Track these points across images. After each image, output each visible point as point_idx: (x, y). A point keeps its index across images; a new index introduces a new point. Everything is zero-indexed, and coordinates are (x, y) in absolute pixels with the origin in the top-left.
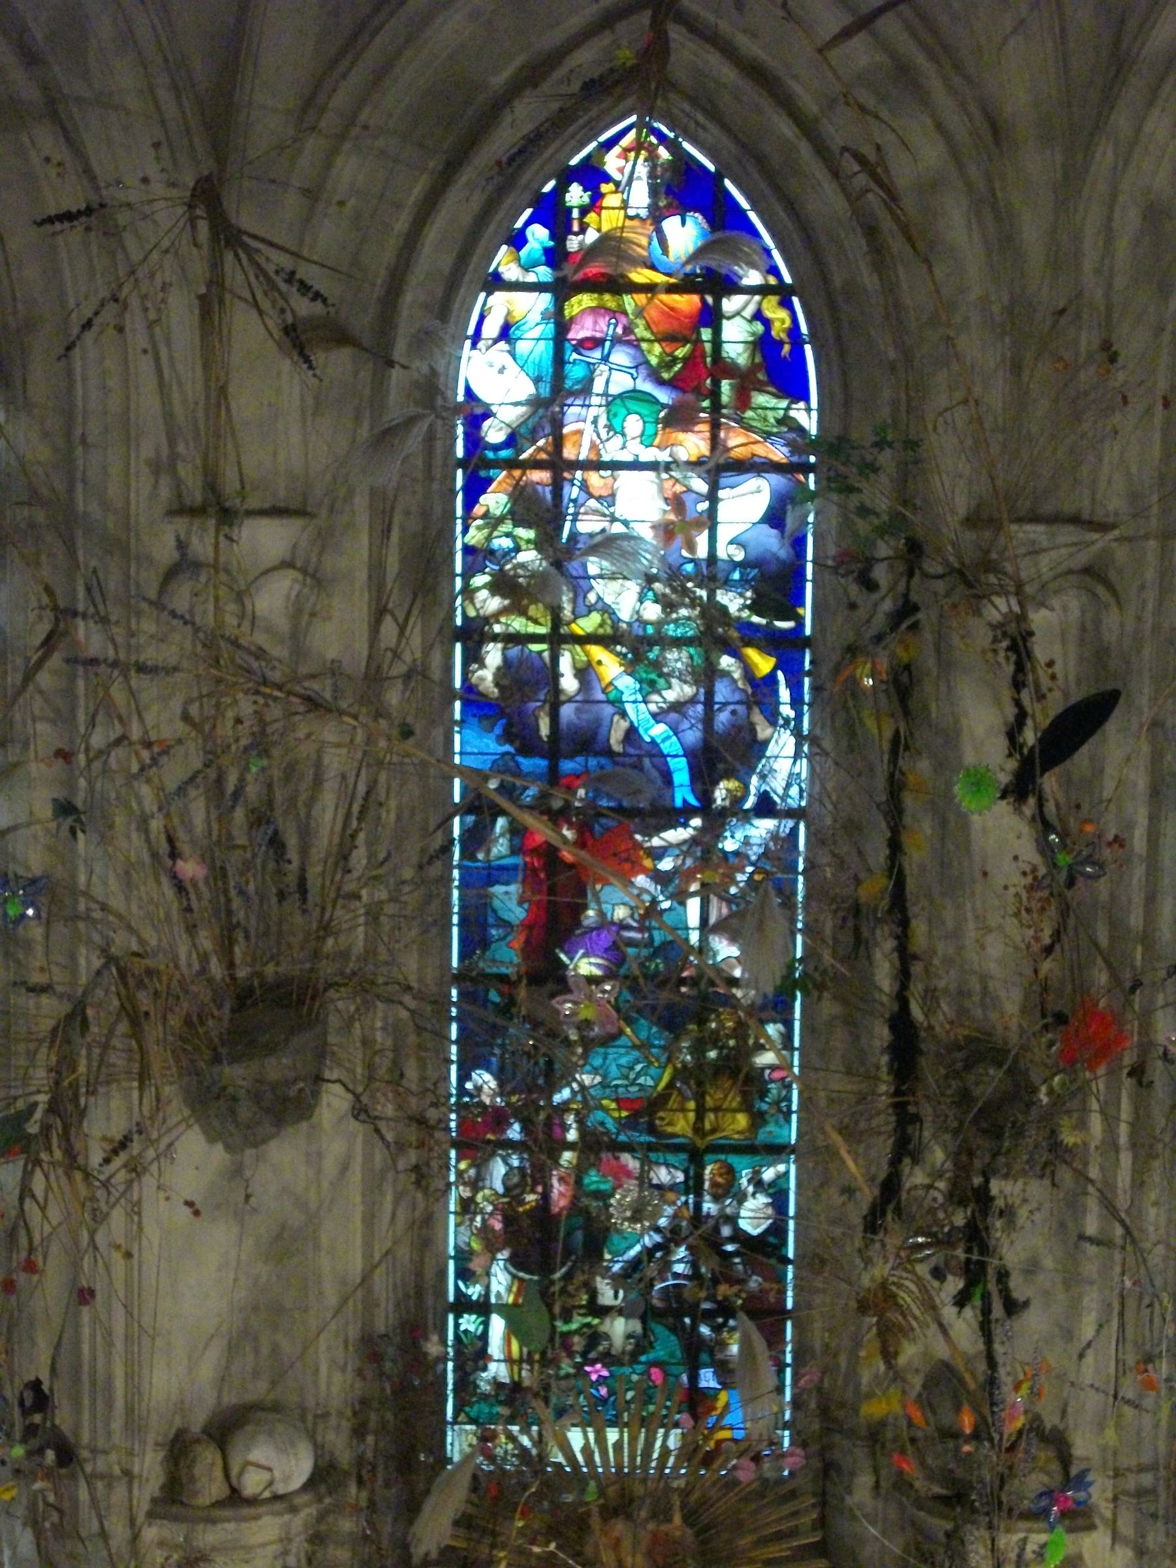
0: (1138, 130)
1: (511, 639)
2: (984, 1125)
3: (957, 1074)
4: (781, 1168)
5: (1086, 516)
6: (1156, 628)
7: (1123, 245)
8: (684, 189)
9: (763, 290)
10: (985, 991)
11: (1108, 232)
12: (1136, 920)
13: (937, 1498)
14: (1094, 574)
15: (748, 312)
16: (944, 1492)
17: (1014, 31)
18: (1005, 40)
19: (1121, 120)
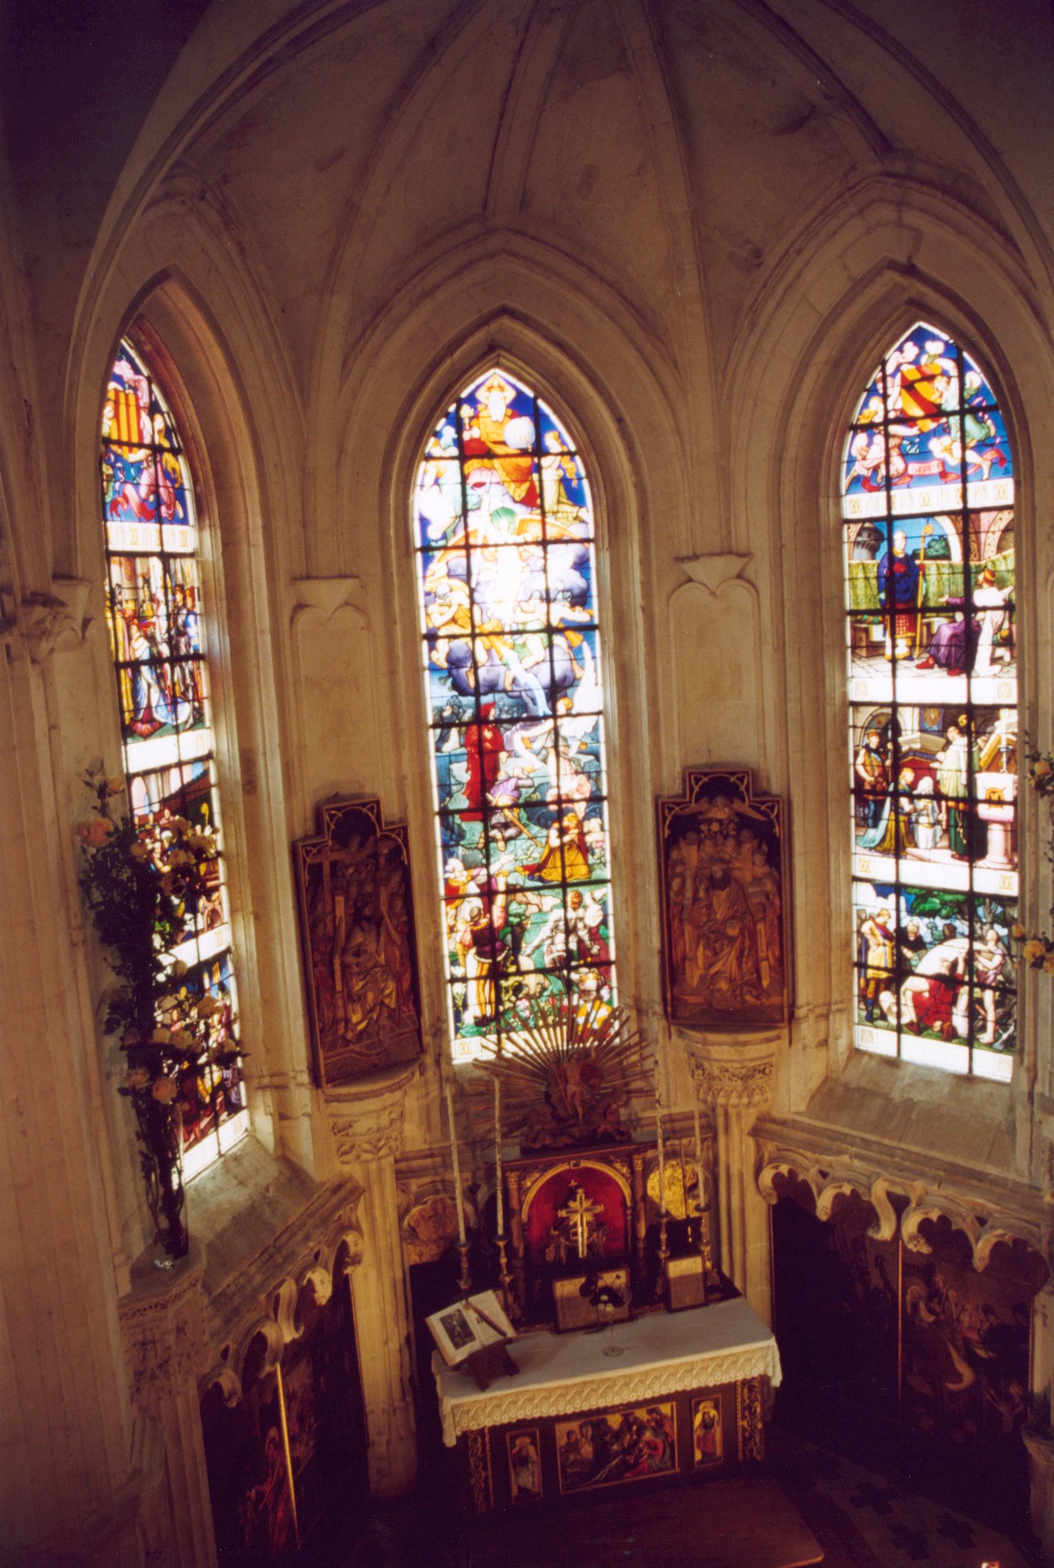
1: (453, 637)
8: (520, 406)
9: (562, 454)
15: (556, 465)
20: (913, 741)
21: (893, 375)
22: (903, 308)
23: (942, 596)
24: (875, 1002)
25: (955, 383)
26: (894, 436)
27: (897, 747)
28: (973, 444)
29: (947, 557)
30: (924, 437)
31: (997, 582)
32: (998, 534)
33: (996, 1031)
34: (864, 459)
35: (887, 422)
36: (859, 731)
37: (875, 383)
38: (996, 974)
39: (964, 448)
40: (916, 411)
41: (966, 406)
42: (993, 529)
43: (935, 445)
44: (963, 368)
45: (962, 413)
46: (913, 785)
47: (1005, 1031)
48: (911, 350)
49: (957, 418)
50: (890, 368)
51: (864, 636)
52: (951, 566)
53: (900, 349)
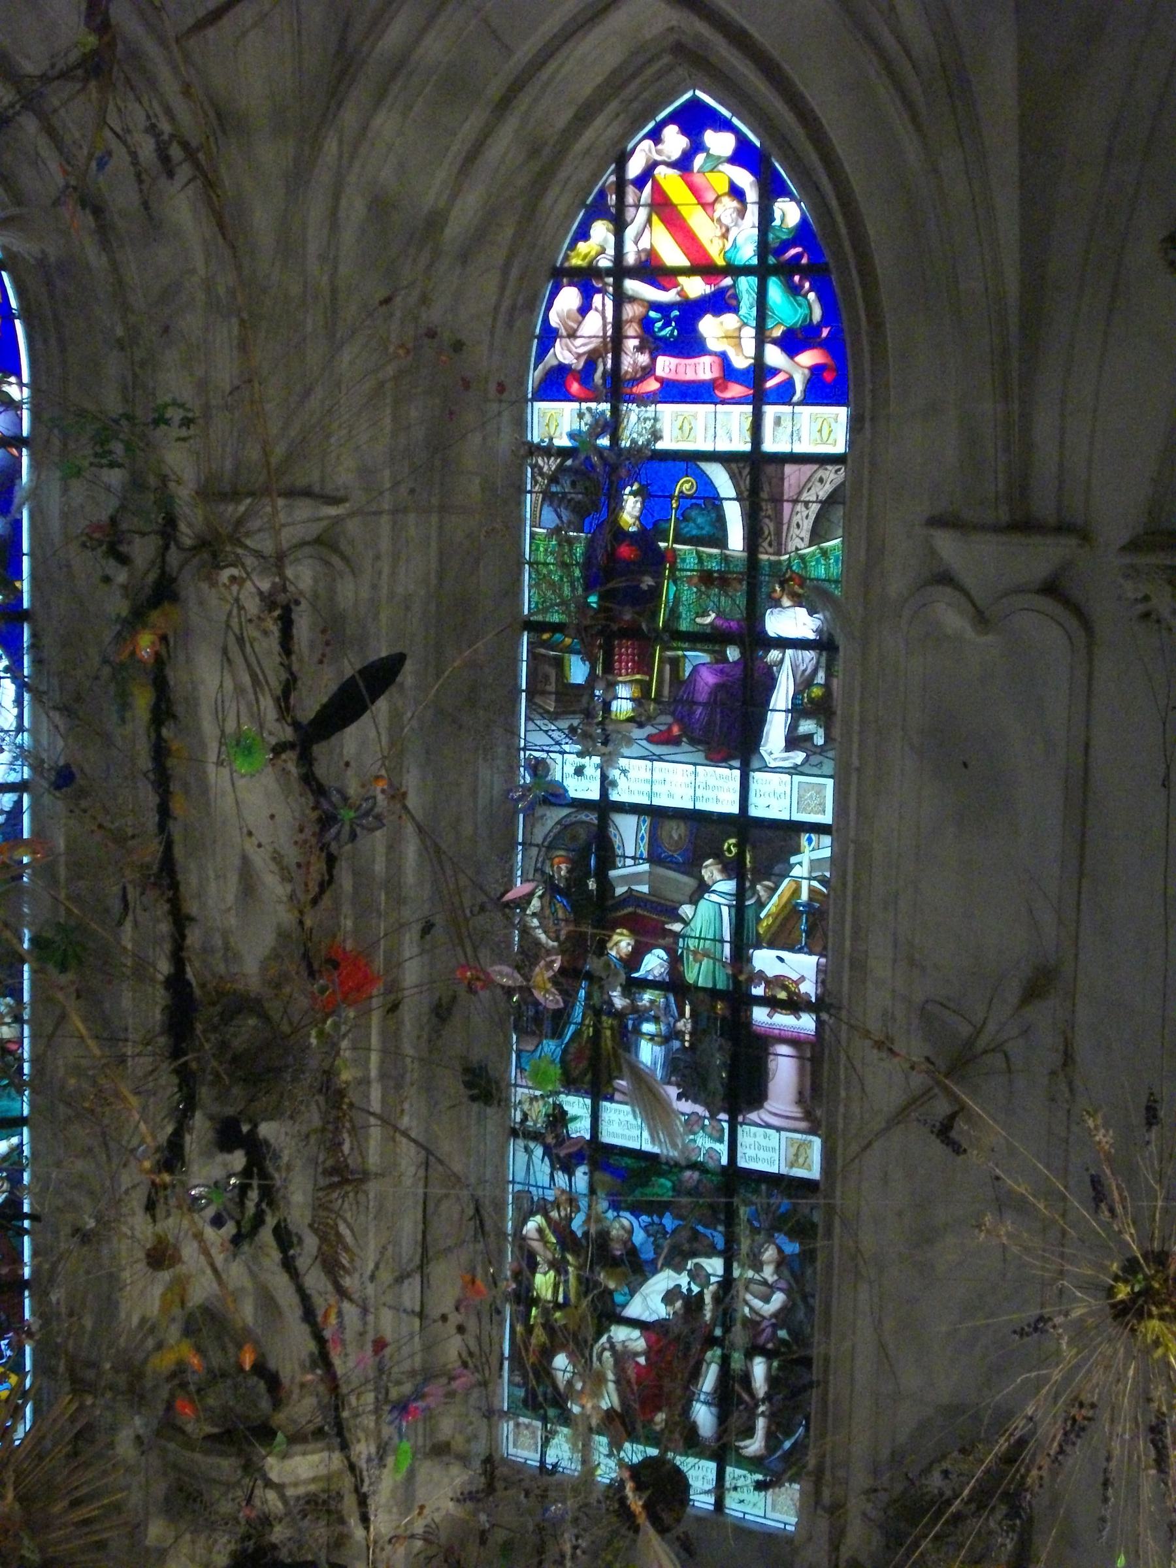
0: (365, 128)
2: (240, 1073)
3: (215, 1029)
4: (15, 1140)
5: (317, 489)
6: (392, 595)
7: (348, 236)
10: (227, 947)
11: (333, 220)
12: (379, 867)
13: (208, 1437)
14: (326, 543)
16: (216, 1430)
17: (255, 25)
18: (244, 34)
19: (349, 117)
20: (636, 878)
21: (640, 182)
22: (667, 59)
23: (705, 614)
24: (544, 1372)
25: (753, 213)
26: (633, 299)
27: (606, 885)
28: (777, 333)
29: (719, 539)
30: (692, 310)
31: (809, 595)
32: (815, 508)
33: (770, 1435)
34: (572, 335)
35: (620, 271)
36: (534, 851)
37: (602, 194)
38: (775, 1327)
39: (761, 339)
40: (673, 255)
41: (772, 260)
42: (805, 496)
43: (710, 327)
44: (771, 189)
45: (761, 272)
46: (634, 960)
47: (788, 1435)
48: (674, 141)
49: (753, 280)
50: (634, 168)
51: (553, 673)
52: (726, 559)
53: (655, 136)
